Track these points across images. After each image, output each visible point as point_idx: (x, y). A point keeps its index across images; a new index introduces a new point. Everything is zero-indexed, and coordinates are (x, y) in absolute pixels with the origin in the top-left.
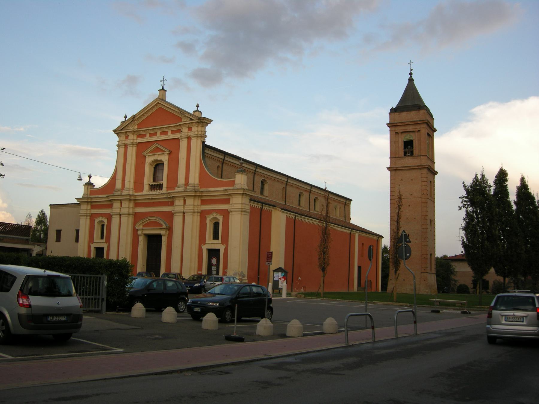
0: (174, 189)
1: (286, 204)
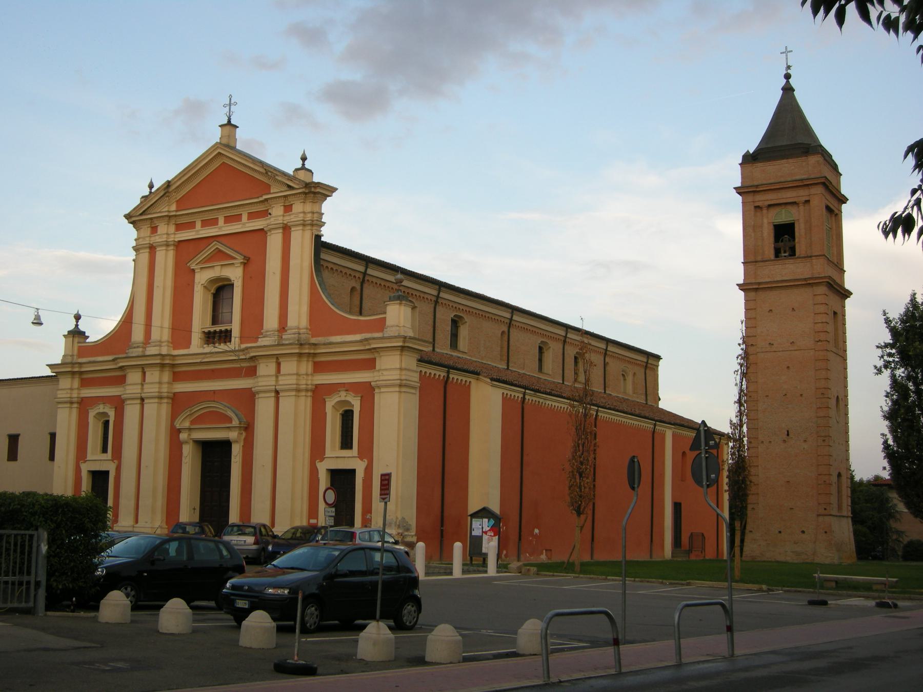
0: (256, 339)
1: (510, 368)
